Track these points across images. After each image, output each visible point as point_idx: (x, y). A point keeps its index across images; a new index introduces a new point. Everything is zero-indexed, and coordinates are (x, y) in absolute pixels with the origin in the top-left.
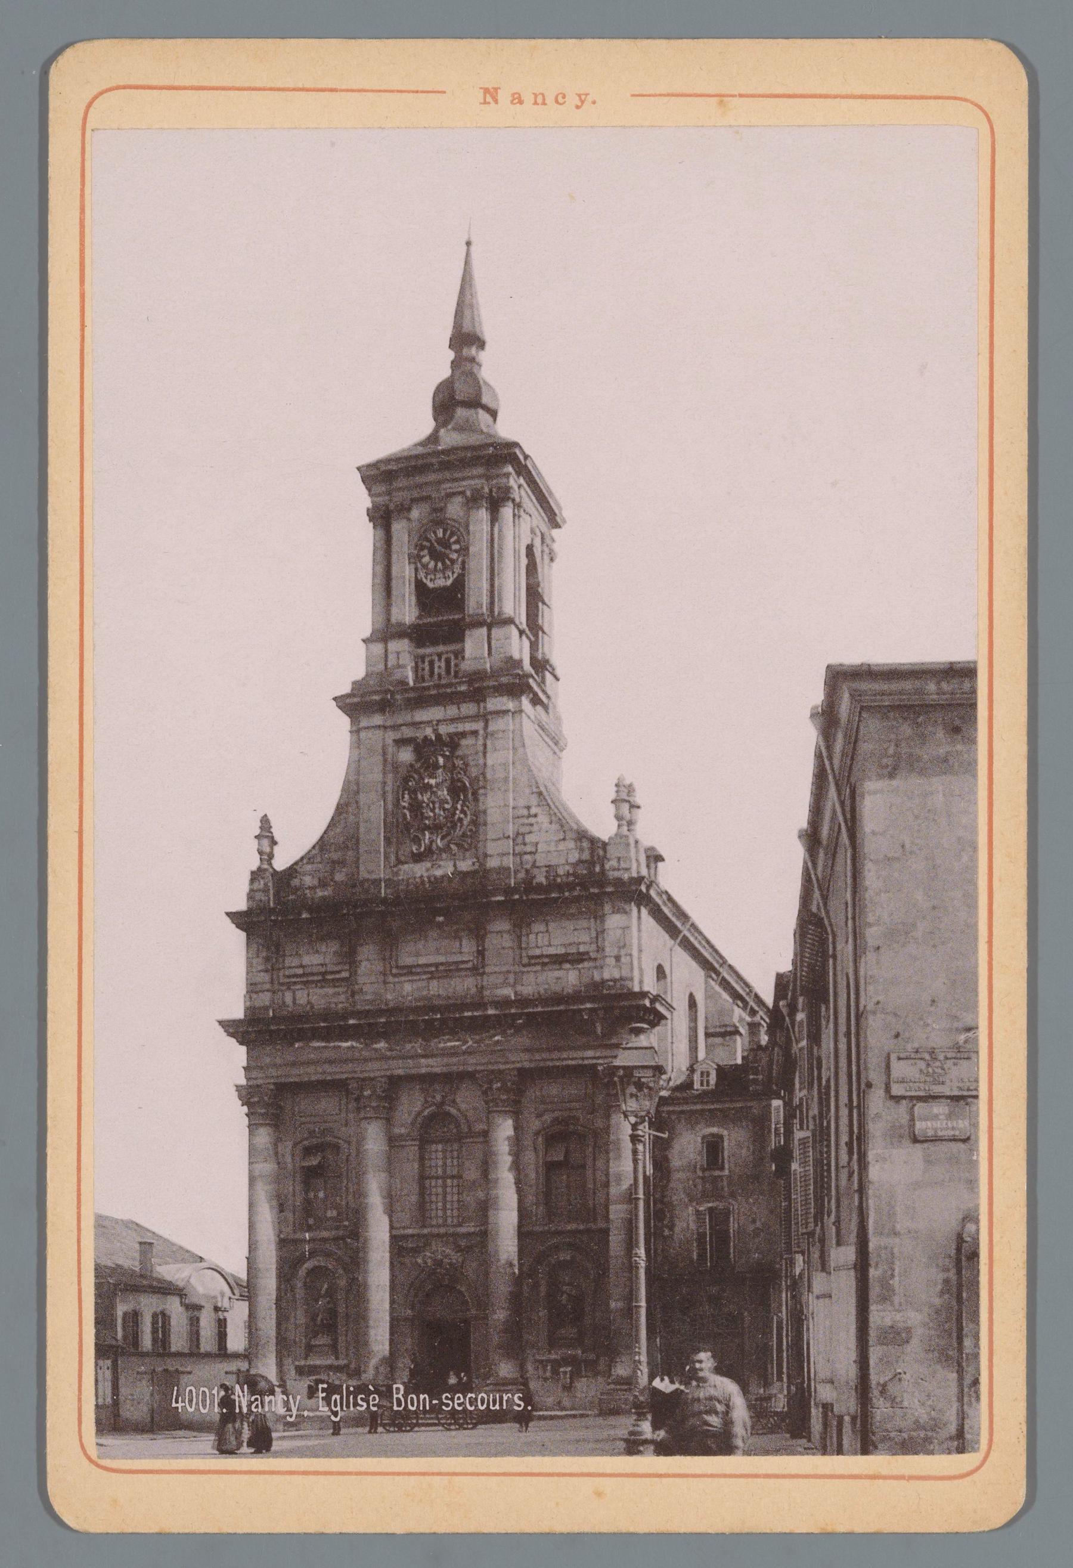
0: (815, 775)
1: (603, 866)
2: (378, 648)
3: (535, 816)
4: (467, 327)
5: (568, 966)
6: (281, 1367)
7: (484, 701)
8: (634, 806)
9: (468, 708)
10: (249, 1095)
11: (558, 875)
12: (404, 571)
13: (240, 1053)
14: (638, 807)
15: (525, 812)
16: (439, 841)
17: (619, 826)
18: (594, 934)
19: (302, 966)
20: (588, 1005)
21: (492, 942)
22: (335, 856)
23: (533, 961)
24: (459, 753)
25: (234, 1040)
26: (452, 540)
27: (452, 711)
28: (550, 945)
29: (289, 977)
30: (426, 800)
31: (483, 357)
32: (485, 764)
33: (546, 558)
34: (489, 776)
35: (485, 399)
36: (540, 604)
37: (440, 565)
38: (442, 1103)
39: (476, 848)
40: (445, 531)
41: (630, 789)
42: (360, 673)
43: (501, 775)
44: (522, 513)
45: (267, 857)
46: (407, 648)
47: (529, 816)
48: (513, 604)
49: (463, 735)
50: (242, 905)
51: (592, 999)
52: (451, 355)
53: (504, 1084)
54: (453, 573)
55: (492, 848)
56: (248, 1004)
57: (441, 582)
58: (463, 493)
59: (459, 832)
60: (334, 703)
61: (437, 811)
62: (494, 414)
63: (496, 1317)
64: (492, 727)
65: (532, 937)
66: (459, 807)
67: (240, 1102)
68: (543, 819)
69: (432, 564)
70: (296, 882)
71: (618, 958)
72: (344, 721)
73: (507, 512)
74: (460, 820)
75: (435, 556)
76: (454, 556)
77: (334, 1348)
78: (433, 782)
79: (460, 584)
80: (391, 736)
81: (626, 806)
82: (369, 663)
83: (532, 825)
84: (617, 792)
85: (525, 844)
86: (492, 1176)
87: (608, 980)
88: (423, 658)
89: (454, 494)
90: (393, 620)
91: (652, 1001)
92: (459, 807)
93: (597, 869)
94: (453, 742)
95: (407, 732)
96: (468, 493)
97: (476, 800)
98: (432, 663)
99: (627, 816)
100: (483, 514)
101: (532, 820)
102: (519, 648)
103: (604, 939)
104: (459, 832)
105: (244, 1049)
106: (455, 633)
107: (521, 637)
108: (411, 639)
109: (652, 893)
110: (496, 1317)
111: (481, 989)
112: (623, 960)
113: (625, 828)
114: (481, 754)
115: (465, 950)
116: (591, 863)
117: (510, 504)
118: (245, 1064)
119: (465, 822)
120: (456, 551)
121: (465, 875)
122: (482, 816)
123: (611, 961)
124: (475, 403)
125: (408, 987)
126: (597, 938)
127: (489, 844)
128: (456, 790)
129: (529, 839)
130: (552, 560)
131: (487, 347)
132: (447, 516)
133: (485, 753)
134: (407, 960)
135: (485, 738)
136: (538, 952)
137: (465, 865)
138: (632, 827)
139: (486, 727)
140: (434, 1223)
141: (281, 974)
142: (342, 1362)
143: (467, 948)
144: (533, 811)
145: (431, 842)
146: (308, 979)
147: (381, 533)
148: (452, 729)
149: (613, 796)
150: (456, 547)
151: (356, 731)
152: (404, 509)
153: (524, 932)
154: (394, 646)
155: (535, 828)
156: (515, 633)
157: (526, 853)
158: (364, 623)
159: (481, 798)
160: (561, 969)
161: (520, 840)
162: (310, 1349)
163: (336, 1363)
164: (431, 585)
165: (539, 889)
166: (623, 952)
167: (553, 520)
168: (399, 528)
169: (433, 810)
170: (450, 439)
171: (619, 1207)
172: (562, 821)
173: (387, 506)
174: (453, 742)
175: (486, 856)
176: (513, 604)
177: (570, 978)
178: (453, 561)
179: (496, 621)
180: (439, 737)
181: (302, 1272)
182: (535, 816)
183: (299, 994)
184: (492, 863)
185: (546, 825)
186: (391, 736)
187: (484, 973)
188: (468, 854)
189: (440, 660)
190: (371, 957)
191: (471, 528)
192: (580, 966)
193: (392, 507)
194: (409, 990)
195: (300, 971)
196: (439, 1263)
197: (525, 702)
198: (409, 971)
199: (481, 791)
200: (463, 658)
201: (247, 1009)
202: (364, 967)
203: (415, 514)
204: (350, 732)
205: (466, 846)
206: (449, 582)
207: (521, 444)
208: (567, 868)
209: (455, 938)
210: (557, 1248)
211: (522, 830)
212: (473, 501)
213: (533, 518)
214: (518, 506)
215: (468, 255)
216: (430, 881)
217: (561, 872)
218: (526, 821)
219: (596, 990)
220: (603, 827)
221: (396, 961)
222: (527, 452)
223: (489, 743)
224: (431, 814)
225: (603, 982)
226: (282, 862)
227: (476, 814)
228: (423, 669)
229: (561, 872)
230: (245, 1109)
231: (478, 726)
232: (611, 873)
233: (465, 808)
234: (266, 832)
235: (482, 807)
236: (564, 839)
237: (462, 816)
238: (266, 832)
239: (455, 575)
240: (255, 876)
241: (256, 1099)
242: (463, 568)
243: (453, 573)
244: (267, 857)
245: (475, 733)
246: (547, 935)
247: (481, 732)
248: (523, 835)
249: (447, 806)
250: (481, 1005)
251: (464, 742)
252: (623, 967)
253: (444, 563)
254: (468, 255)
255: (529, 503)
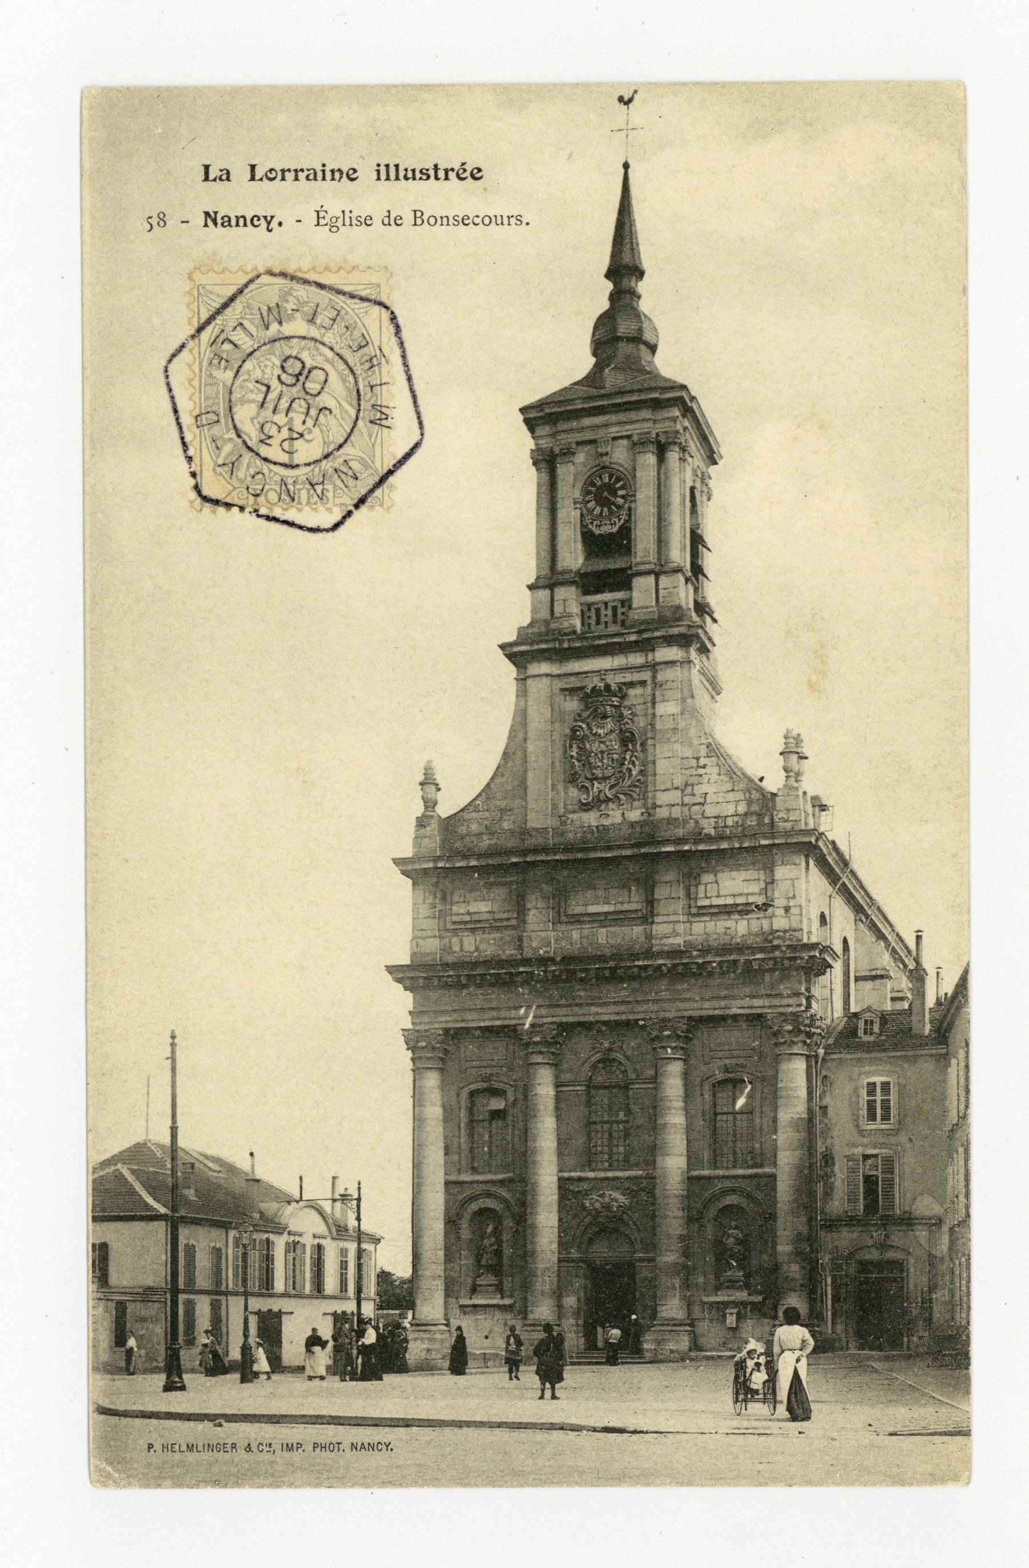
0: (618, 1485)
1: (772, 816)
2: (544, 594)
3: (704, 767)
4: (627, 259)
5: (736, 916)
6: (705, 1020)
7: (653, 650)
8: (803, 758)
9: (637, 659)
10: (414, 1042)
11: (726, 826)
12: (569, 515)
13: (406, 1000)
14: (806, 758)
15: (694, 763)
16: (607, 790)
17: (787, 777)
18: (763, 885)
19: (469, 913)
20: (758, 956)
21: (661, 892)
22: (502, 804)
23: (701, 912)
24: (627, 703)
25: (400, 986)
26: (618, 485)
27: (619, 661)
28: (718, 896)
29: (454, 923)
30: (594, 750)
31: (642, 287)
32: (654, 714)
33: (705, 498)
34: (658, 727)
35: (648, 336)
36: (700, 547)
37: (606, 510)
38: (610, 1050)
39: (645, 799)
40: (611, 477)
41: (798, 740)
42: (526, 621)
43: (670, 725)
44: (687, 457)
45: (430, 804)
46: (574, 596)
47: (699, 767)
48: (679, 554)
49: (631, 685)
50: (407, 851)
51: (762, 950)
52: (609, 286)
53: (674, 1029)
54: (619, 520)
55: (663, 798)
56: (432, 945)
57: (607, 529)
58: (629, 437)
59: (627, 782)
60: (500, 652)
61: (605, 761)
62: (653, 349)
63: (665, 1259)
64: (660, 677)
65: (701, 888)
66: (628, 757)
67: (405, 1046)
68: (712, 771)
69: (598, 509)
70: (462, 830)
71: (787, 909)
72: (510, 670)
73: (673, 456)
74: (630, 770)
75: (602, 502)
76: (620, 501)
77: (499, 1289)
78: (601, 731)
79: (626, 531)
80: (559, 684)
81: (795, 757)
82: (534, 610)
83: (701, 776)
84: (785, 744)
85: (693, 795)
86: (660, 1121)
87: (777, 931)
88: (589, 606)
89: (621, 437)
90: (560, 566)
91: (821, 952)
92: (628, 757)
93: (767, 820)
94: (622, 691)
95: (573, 682)
96: (635, 438)
97: (644, 750)
98: (598, 610)
99: (796, 768)
100: (651, 459)
101: (701, 771)
102: (684, 596)
103: (773, 890)
104: (627, 782)
105: (409, 995)
106: (622, 580)
107: (686, 583)
108: (577, 587)
109: (821, 844)
110: (665, 1259)
111: (649, 937)
112: (793, 911)
113: (793, 779)
114: (649, 704)
115: (633, 899)
116: (760, 815)
117: (677, 448)
118: (411, 1008)
119: (634, 773)
120: (623, 497)
121: (633, 825)
122: (651, 766)
123: (781, 912)
124: (637, 339)
125: (575, 935)
126: (766, 889)
127: (658, 794)
128: (627, 739)
129: (699, 790)
130: (709, 499)
131: (646, 276)
132: (614, 460)
133: (654, 703)
134: (577, 908)
135: (654, 689)
136: (706, 902)
137: (635, 815)
138: (800, 778)
139: (654, 677)
140: (600, 1166)
141: (448, 918)
142: (507, 1301)
143: (634, 902)
144: (702, 761)
145: (600, 792)
146: (473, 925)
147: (545, 477)
148: (620, 678)
149: (781, 748)
150: (621, 493)
151: (522, 680)
152: (568, 453)
153: (693, 882)
154: (561, 593)
155: (706, 778)
156: (682, 580)
157: (695, 804)
158: (529, 569)
159: (650, 749)
160: (729, 919)
161: (689, 790)
162: (474, 1290)
163: (501, 1302)
164: (597, 532)
165: (709, 839)
166: (792, 903)
167: (712, 459)
168: (566, 472)
169: (601, 761)
170: (612, 379)
171: (787, 1153)
172: (732, 772)
173: (552, 451)
174: (622, 691)
175: (655, 806)
176: (679, 554)
177: (741, 927)
178: (619, 507)
179: (661, 570)
180: (607, 687)
181: (467, 1215)
182: (704, 767)
183: (466, 941)
184: (662, 813)
185: (714, 777)
186: (559, 684)
187: (653, 922)
188: (636, 804)
189: (606, 608)
190: (539, 905)
191: (638, 474)
192: (749, 916)
193: (557, 450)
194: (576, 938)
195: (468, 918)
196: (607, 1207)
197: (693, 654)
198: (577, 920)
199: (650, 742)
200: (630, 607)
201: (413, 955)
202: (532, 916)
203: (580, 457)
204: (516, 679)
205: (635, 795)
206: (615, 529)
207: (689, 387)
208: (736, 819)
209: (623, 887)
210: (725, 1192)
211: (692, 780)
212: (637, 445)
213: (697, 460)
214: (684, 449)
215: (626, 175)
216: (598, 830)
217: (730, 822)
218: (694, 772)
219: (768, 942)
220: (774, 782)
221: (565, 912)
222: (693, 393)
223: (657, 693)
224: (600, 764)
225: (773, 932)
226: (445, 810)
227: (644, 764)
228: (589, 617)
229: (730, 822)
230: (410, 1054)
231: (646, 675)
232: (781, 824)
233: (634, 759)
234: (429, 781)
235: (650, 758)
236: (733, 790)
237: (631, 766)
238: (429, 781)
239: (622, 521)
240: (421, 823)
241: (424, 1044)
242: (630, 515)
243: (619, 520)
244: (430, 804)
245: (643, 683)
246: (715, 885)
247: (649, 682)
248: (692, 785)
249: (615, 756)
250: (648, 954)
251: (632, 692)
252: (792, 917)
253: (610, 509)
254: (626, 175)
255: (693, 445)
